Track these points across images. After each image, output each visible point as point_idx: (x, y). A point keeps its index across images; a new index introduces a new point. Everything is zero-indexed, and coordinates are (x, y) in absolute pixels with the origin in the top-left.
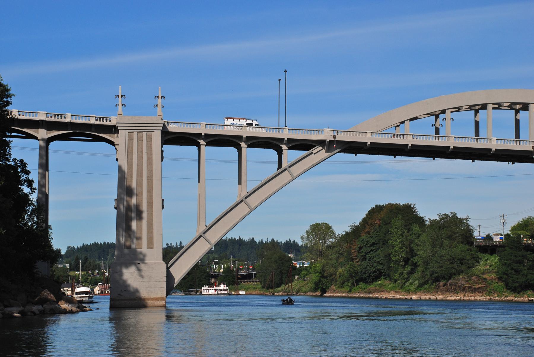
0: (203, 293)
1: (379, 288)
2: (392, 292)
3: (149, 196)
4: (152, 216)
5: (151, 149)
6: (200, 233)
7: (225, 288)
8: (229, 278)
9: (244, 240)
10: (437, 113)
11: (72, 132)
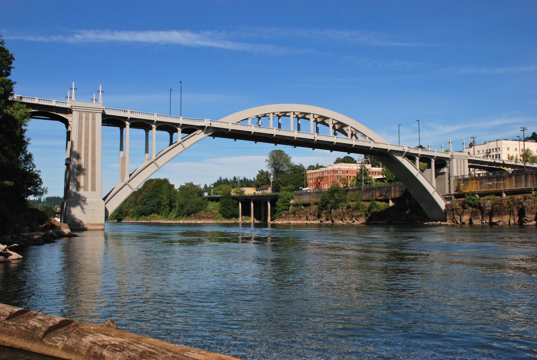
2: (162, 220)
10: (260, 116)
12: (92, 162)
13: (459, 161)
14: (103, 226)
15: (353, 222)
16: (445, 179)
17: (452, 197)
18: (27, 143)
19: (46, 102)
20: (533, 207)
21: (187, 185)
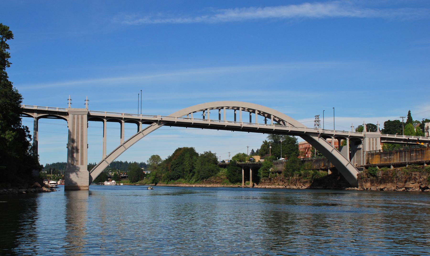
2: (185, 184)
7: (114, 182)
10: (204, 110)
13: (371, 139)
14: (88, 188)
15: (301, 187)
16: (361, 154)
17: (363, 168)
20: (403, 177)
21: (205, 154)
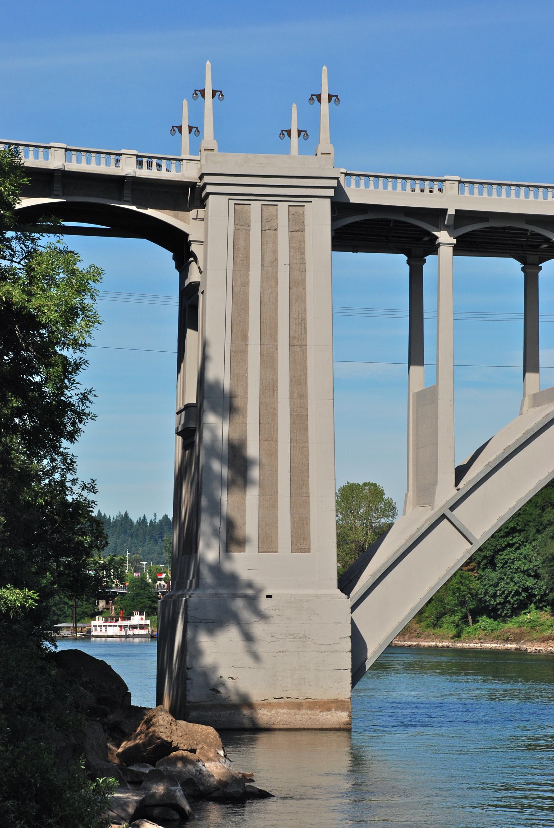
0: (92, 633)
1: (529, 630)
3: (295, 396)
4: (307, 456)
5: (303, 253)
6: (441, 508)
7: (143, 622)
8: (142, 600)
9: (108, 517)
11: (65, 201)
12: (262, 392)
18: (80, 415)
19: (89, 162)
